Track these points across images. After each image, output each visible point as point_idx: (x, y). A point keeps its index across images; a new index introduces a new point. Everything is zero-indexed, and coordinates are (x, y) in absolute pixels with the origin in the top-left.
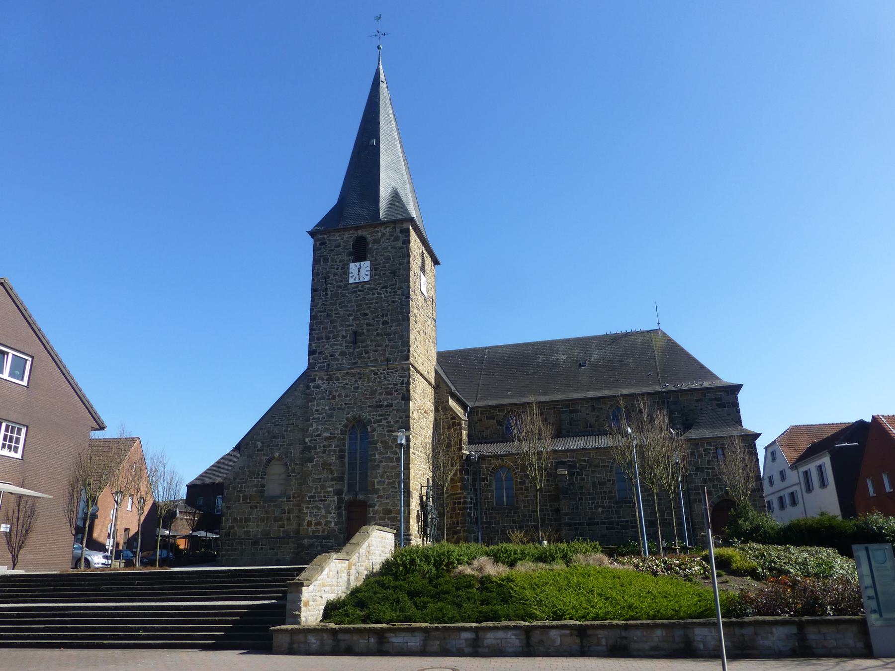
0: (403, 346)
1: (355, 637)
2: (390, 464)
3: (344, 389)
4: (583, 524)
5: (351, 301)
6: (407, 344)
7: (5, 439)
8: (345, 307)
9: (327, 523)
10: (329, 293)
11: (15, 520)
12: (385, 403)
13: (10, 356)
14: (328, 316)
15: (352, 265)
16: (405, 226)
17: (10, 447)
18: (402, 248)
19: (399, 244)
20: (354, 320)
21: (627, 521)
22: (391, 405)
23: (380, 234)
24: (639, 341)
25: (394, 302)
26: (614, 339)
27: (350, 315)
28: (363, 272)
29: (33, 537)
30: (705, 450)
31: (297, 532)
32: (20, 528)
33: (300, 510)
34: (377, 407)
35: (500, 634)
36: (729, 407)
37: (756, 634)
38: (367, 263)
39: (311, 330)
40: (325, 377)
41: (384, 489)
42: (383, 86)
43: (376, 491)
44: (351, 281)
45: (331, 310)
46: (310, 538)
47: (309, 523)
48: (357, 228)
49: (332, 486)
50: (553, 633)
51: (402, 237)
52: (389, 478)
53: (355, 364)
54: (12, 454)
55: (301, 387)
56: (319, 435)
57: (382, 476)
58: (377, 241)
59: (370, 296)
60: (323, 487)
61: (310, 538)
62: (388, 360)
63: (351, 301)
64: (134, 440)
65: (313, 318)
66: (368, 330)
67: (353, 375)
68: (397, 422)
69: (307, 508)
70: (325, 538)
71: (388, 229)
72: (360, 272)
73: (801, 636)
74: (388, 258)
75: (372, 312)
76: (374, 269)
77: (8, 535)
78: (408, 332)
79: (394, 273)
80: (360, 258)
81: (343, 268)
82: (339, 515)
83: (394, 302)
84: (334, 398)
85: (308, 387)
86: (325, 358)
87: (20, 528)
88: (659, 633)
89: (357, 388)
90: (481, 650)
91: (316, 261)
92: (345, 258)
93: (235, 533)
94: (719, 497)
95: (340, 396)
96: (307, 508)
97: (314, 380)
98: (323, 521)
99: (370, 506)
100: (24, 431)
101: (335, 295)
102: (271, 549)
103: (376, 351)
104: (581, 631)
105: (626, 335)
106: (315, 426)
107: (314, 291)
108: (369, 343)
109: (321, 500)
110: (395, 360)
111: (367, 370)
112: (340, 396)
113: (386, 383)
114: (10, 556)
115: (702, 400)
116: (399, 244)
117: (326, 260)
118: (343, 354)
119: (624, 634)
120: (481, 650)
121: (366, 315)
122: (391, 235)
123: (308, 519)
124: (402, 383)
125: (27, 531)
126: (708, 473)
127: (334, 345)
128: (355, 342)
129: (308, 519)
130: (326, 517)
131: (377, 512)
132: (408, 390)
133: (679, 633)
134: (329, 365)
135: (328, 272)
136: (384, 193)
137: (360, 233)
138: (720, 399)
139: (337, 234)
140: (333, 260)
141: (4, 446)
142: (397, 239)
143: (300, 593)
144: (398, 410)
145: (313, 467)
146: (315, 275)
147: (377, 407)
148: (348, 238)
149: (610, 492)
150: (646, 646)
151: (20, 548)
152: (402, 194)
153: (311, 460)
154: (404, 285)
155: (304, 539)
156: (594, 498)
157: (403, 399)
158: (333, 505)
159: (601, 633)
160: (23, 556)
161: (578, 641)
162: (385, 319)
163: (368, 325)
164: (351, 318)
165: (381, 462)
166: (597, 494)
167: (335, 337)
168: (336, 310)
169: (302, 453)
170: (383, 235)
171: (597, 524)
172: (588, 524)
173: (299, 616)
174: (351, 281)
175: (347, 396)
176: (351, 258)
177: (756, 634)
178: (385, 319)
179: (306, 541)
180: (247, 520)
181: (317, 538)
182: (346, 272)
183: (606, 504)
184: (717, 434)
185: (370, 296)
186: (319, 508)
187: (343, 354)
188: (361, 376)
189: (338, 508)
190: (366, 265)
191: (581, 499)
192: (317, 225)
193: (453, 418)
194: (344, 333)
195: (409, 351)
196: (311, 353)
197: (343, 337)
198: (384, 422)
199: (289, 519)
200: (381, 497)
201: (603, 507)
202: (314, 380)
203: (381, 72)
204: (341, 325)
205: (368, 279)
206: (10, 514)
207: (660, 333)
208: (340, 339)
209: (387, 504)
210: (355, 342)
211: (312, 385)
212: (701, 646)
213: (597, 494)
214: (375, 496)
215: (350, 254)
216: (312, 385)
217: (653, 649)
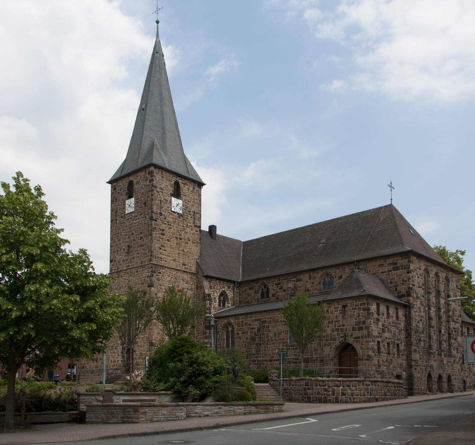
4: (266, 361)
9: (118, 361)
10: (118, 222)
20: (129, 238)
21: (291, 359)
23: (139, 177)
25: (145, 224)
27: (126, 235)
30: (335, 308)
36: (402, 269)
39: (111, 247)
44: (127, 212)
46: (111, 369)
53: (128, 266)
58: (138, 183)
63: (127, 226)
65: (112, 239)
66: (134, 244)
69: (111, 353)
70: (117, 369)
72: (130, 205)
76: (136, 203)
80: (130, 197)
81: (123, 204)
82: (123, 357)
92: (125, 197)
94: (340, 342)
96: (111, 353)
98: (116, 360)
102: (98, 375)
107: (112, 221)
109: (116, 348)
112: (122, 287)
113: (141, 277)
121: (133, 234)
122: (144, 177)
126: (335, 324)
127: (120, 255)
129: (111, 359)
130: (118, 358)
138: (396, 264)
146: (112, 210)
149: (284, 339)
156: (274, 343)
158: (120, 351)
162: (141, 235)
163: (134, 240)
164: (127, 237)
166: (276, 341)
171: (275, 360)
172: (270, 361)
174: (127, 212)
178: (141, 235)
183: (281, 347)
191: (267, 344)
194: (124, 247)
196: (111, 261)
197: (124, 250)
201: (279, 349)
204: (123, 243)
208: (122, 251)
209: (141, 350)
213: (276, 341)
214: (136, 345)
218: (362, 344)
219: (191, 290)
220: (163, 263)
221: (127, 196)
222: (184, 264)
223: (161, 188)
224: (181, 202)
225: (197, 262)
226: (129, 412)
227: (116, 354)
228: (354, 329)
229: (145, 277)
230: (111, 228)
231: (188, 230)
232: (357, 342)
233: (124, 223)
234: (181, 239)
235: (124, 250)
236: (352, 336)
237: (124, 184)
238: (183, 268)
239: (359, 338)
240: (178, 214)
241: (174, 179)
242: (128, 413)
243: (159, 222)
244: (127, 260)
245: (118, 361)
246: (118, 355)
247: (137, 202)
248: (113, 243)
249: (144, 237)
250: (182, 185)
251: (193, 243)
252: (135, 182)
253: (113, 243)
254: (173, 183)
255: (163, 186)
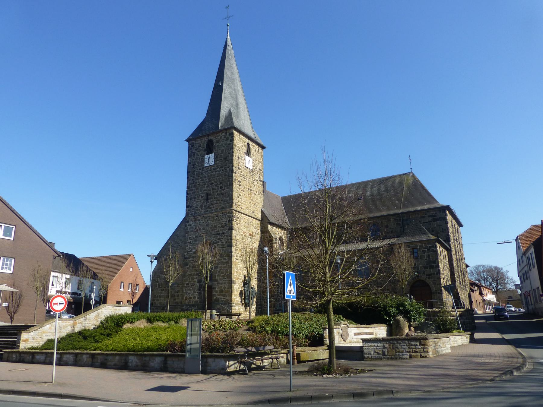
0: (230, 200)
1: (26, 355)
2: (223, 266)
3: (202, 225)
5: (205, 177)
6: (231, 199)
7: (3, 264)
8: (203, 180)
9: (194, 297)
10: (195, 173)
11: (11, 301)
12: (221, 232)
13: (3, 227)
14: (195, 186)
15: (206, 157)
16: (231, 131)
17: (6, 268)
18: (230, 144)
19: (228, 142)
20: (207, 187)
22: (223, 233)
24: (397, 181)
25: (225, 175)
26: (383, 181)
27: (205, 184)
28: (211, 159)
29: (21, 308)
31: (181, 303)
32: (14, 304)
33: (183, 291)
34: (217, 234)
35: (68, 356)
36: (441, 220)
37: (150, 360)
38: (213, 154)
39: (187, 194)
40: (193, 220)
41: (220, 279)
42: (230, 48)
43: (216, 280)
44: (205, 165)
45: (196, 183)
46: (187, 305)
47: (186, 298)
48: (208, 135)
49: (196, 278)
50: (84, 356)
51: (230, 138)
52: (222, 273)
53: (207, 211)
54: (8, 271)
55: (183, 226)
56: (191, 251)
57: (219, 272)
58: (218, 142)
59: (214, 173)
60: (193, 279)
61: (187, 305)
62: (222, 208)
63: (205, 177)
64: (130, 255)
65: (188, 187)
66: (213, 192)
67: (206, 218)
68: (226, 242)
71: (223, 134)
72: (210, 160)
73: (165, 362)
74: (223, 150)
75: (215, 182)
76: (216, 158)
77: (7, 308)
78: (232, 191)
79: (225, 159)
80: (209, 152)
81: (202, 159)
83: (225, 175)
84: (197, 231)
85: (186, 226)
86: (194, 209)
87: (14, 304)
88: (117, 358)
89: (208, 225)
90: (61, 363)
91: (189, 156)
92: (203, 153)
93: (155, 303)
95: (200, 229)
97: (188, 222)
98: (192, 297)
99: (213, 289)
100: (13, 260)
101: (198, 174)
103: (217, 203)
104: (93, 356)
105: (391, 178)
106: (189, 246)
107: (188, 172)
108: (214, 199)
110: (225, 208)
111: (213, 214)
112: (200, 229)
114: (9, 317)
115: (424, 217)
116: (228, 142)
117: (194, 155)
118: (201, 206)
119: (106, 358)
120: (61, 363)
121: (212, 184)
122: (225, 137)
123: (186, 295)
124: (229, 221)
125: (18, 306)
127: (198, 202)
128: (207, 199)
129: (186, 295)
130: (194, 295)
131: (216, 292)
132: (232, 224)
133: (124, 358)
134: (195, 213)
135: (195, 162)
136: (223, 113)
137: (210, 138)
138: (435, 216)
139: (199, 140)
140: (197, 154)
141: (2, 268)
142: (227, 139)
143: (21, 336)
144: (227, 236)
145: (188, 268)
146: (189, 163)
147: (217, 234)
148: (204, 141)
150: (113, 364)
151: (15, 313)
152: (233, 112)
153: (187, 265)
154: (230, 165)
155: (183, 306)
157: (229, 230)
158: (197, 288)
159: (99, 357)
160: (15, 317)
161: (91, 359)
162: (221, 185)
163: (213, 189)
165: (219, 264)
167: (198, 197)
168: (199, 182)
169: (183, 261)
170: (221, 137)
173: (19, 346)
174: (205, 165)
175: (203, 229)
176: (206, 152)
177: (150, 360)
178: (221, 185)
179: (184, 307)
180: (160, 297)
181: (190, 306)
182: (203, 161)
184: (413, 240)
185: (214, 173)
186: (191, 290)
187: (201, 206)
188: (210, 218)
189: (199, 290)
190: (212, 155)
192: (191, 136)
193: (270, 237)
194: (202, 195)
195: (232, 202)
196: (187, 207)
197: (202, 197)
198: (220, 243)
199: (178, 296)
200: (219, 283)
202: (188, 222)
203: (229, 40)
204: (201, 191)
205: (213, 163)
206: (8, 298)
207: (411, 174)
210: (207, 199)
211: (187, 224)
212: (130, 365)
215: (205, 151)
216: (187, 224)
217: (115, 365)
218: (434, 280)
219: (258, 234)
220: (240, 209)
221: (206, 152)
222: (253, 212)
223: (239, 148)
224: (251, 159)
225: (262, 211)
226: (416, 345)
227: (192, 291)
228: (425, 268)
229: (226, 221)
230: (188, 178)
231: (256, 183)
232: (429, 278)
233: (202, 174)
234: (251, 190)
235: (202, 197)
236: (424, 273)
237: (203, 142)
238: (252, 215)
239: (431, 275)
240: (250, 169)
241: (247, 141)
242: (414, 347)
243: (238, 174)
244: (205, 206)
245: (194, 297)
246: (195, 292)
247: (217, 157)
248: (190, 190)
249: (225, 186)
250: (251, 147)
251: (259, 194)
252: (214, 140)
253: (190, 190)
254: (246, 144)
255: (240, 146)
